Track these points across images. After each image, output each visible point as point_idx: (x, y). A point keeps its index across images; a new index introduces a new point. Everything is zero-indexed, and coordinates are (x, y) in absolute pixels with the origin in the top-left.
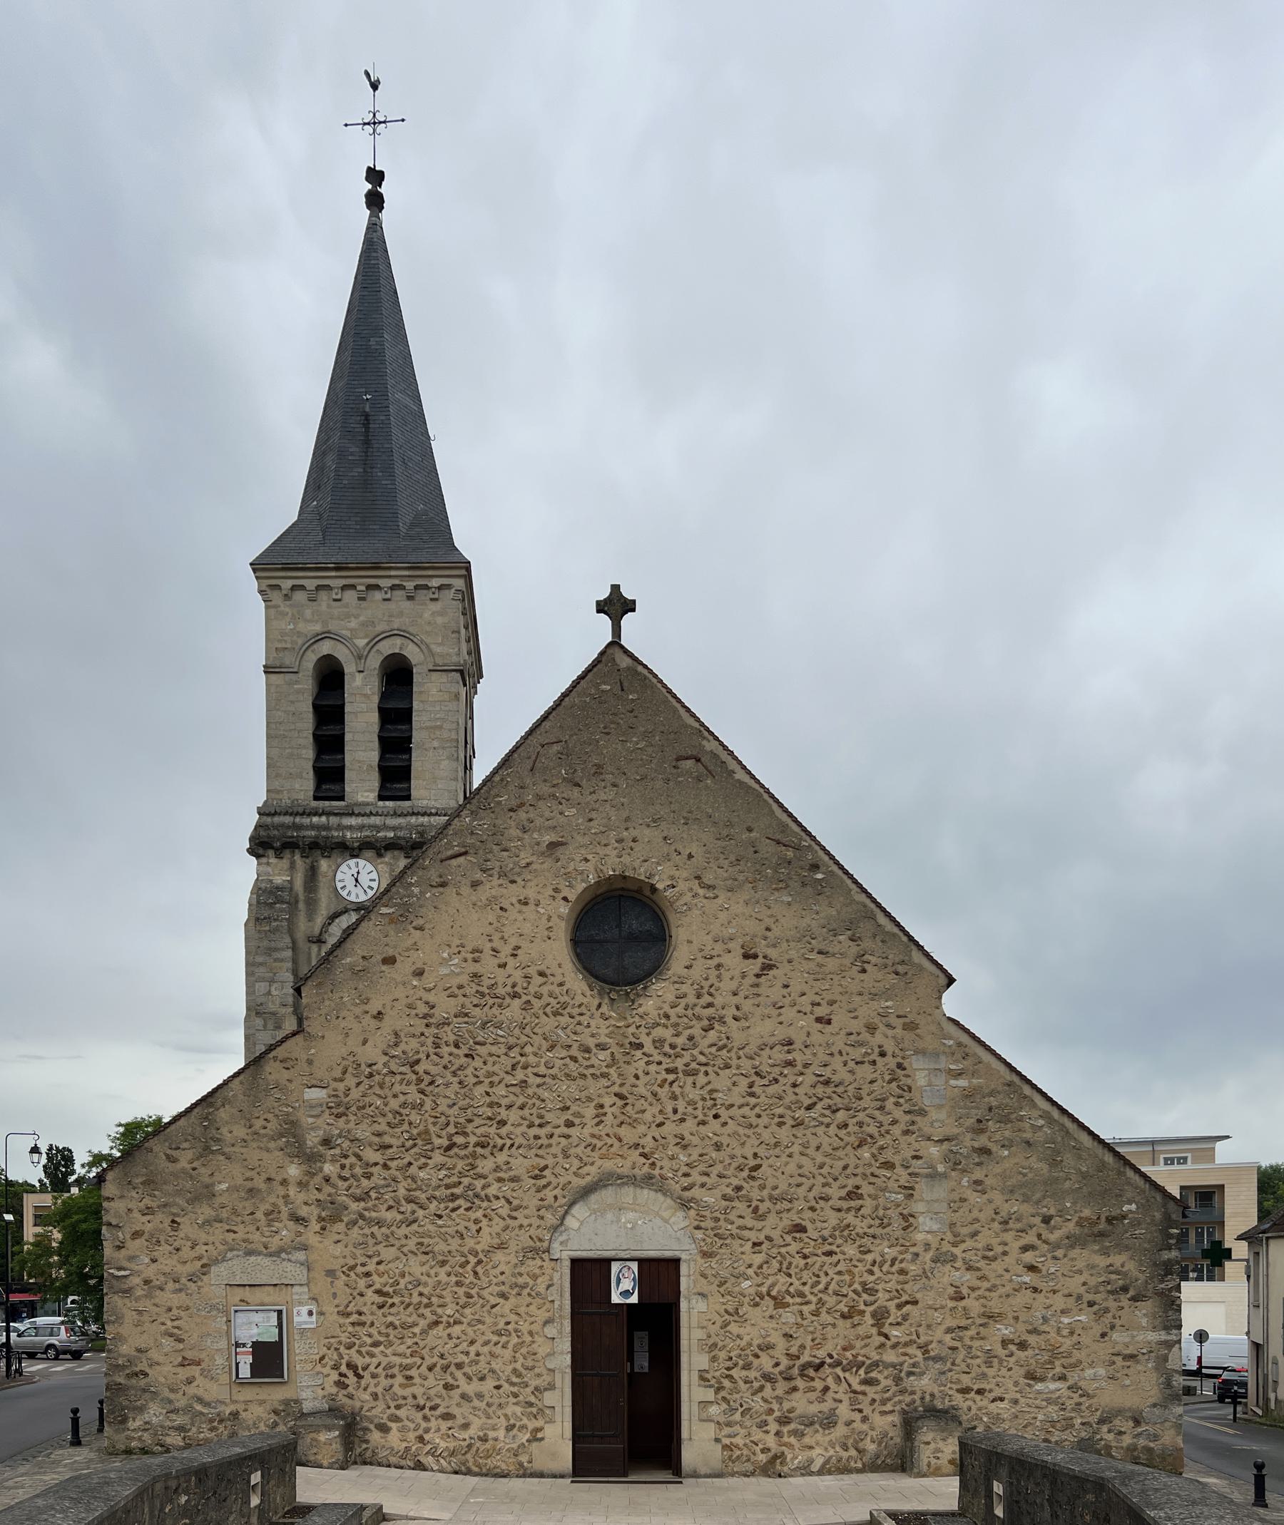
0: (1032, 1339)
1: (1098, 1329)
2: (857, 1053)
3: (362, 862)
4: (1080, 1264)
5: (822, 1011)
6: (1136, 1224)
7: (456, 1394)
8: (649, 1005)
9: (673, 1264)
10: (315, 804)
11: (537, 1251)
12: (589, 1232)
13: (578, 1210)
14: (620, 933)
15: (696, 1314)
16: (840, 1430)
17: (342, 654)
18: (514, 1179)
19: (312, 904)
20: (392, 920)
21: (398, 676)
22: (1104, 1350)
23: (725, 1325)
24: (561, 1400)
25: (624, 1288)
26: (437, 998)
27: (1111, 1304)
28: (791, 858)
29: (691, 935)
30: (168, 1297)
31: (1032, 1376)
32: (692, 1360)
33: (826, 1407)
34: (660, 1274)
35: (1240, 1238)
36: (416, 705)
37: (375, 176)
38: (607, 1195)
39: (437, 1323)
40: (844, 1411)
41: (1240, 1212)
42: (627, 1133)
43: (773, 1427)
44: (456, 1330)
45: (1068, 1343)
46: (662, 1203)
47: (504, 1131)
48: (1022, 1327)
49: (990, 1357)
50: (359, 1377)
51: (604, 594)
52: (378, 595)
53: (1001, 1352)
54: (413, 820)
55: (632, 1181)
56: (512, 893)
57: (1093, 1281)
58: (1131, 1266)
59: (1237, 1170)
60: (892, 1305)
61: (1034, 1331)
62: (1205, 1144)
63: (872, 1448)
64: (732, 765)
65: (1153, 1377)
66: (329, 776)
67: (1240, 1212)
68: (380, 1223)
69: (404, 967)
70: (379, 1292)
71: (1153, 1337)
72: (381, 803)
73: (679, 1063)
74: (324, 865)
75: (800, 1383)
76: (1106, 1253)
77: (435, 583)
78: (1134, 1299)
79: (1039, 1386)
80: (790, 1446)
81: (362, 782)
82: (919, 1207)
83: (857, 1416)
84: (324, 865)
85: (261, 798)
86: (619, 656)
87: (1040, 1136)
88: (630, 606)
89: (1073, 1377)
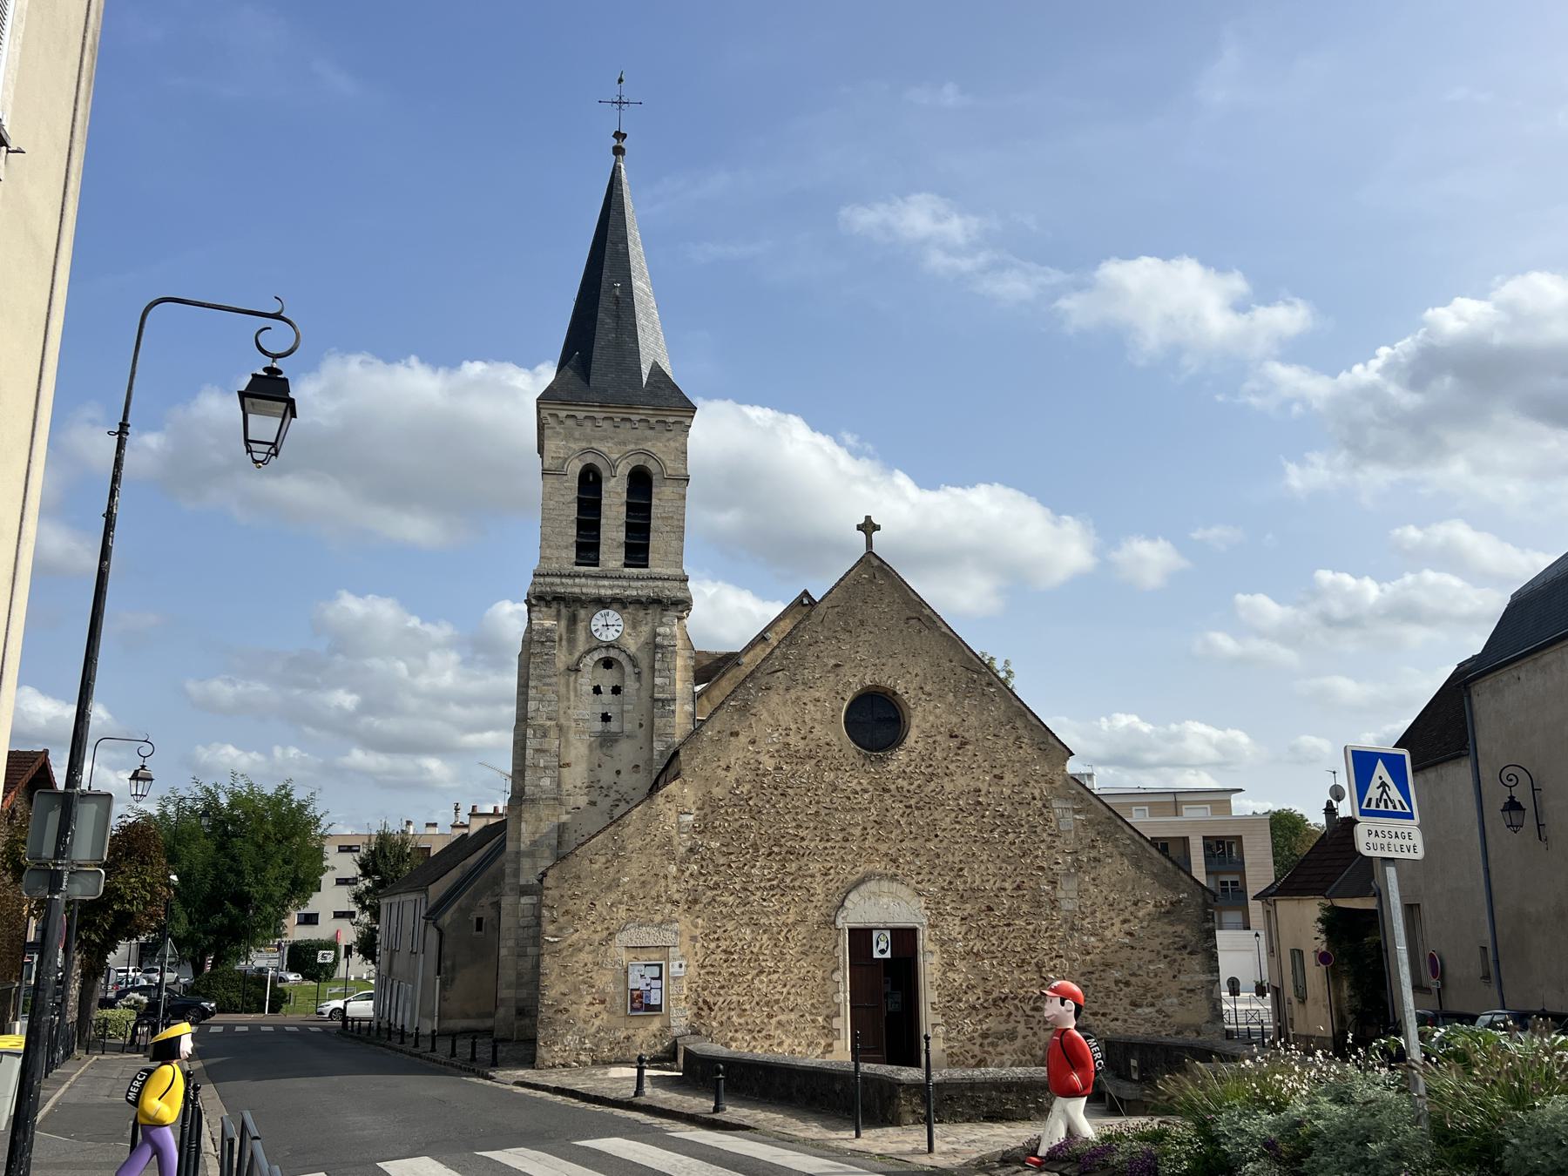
0: (1133, 980)
1: (1171, 973)
2: (1017, 798)
3: (611, 612)
4: (1157, 931)
5: (997, 772)
6: (1188, 906)
7: (773, 1021)
8: (893, 766)
9: (914, 931)
10: (577, 568)
11: (829, 922)
12: (863, 910)
13: (853, 896)
14: (876, 720)
15: (930, 966)
16: (1019, 1042)
17: (600, 463)
18: (812, 876)
19: (572, 642)
20: (737, 709)
21: (640, 482)
22: (1175, 986)
23: (944, 973)
24: (844, 1023)
25: (881, 949)
26: (764, 758)
27: (1178, 957)
28: (979, 678)
29: (921, 722)
30: (585, 957)
31: (1134, 1004)
32: (929, 996)
33: (1010, 1026)
34: (905, 939)
35: (1255, 898)
36: (654, 502)
37: (619, 135)
38: (872, 886)
39: (762, 972)
40: (1021, 1028)
41: (1260, 870)
42: (883, 848)
43: (979, 1041)
44: (775, 977)
45: (1154, 982)
46: (905, 892)
47: (804, 844)
48: (1126, 972)
49: (1108, 993)
50: (711, 1009)
51: (862, 521)
52: (628, 425)
53: (1115, 989)
54: (651, 583)
55: (881, 877)
56: (807, 696)
57: (1166, 942)
58: (1187, 933)
59: (1252, 821)
60: (1046, 959)
61: (1133, 975)
62: (1219, 799)
63: (1040, 1053)
64: (940, 624)
65: (1205, 1003)
66: (588, 549)
67: (1260, 870)
68: (725, 905)
69: (743, 739)
70: (725, 951)
71: (1203, 977)
72: (627, 570)
73: (912, 802)
74: (582, 613)
75: (993, 1011)
76: (1171, 924)
77: (671, 420)
78: (1191, 953)
79: (1139, 1011)
80: (988, 1053)
81: (612, 555)
82: (1061, 894)
83: (1030, 1032)
84: (582, 613)
85: (534, 563)
86: (873, 559)
87: (1128, 851)
88: (877, 528)
89: (1159, 1004)
